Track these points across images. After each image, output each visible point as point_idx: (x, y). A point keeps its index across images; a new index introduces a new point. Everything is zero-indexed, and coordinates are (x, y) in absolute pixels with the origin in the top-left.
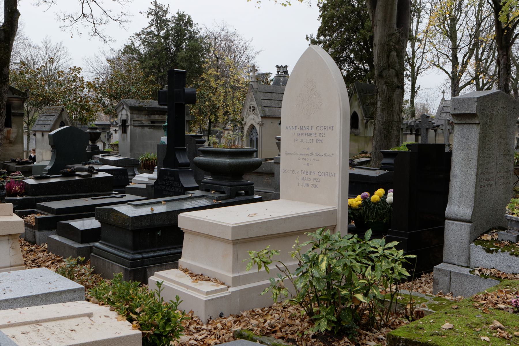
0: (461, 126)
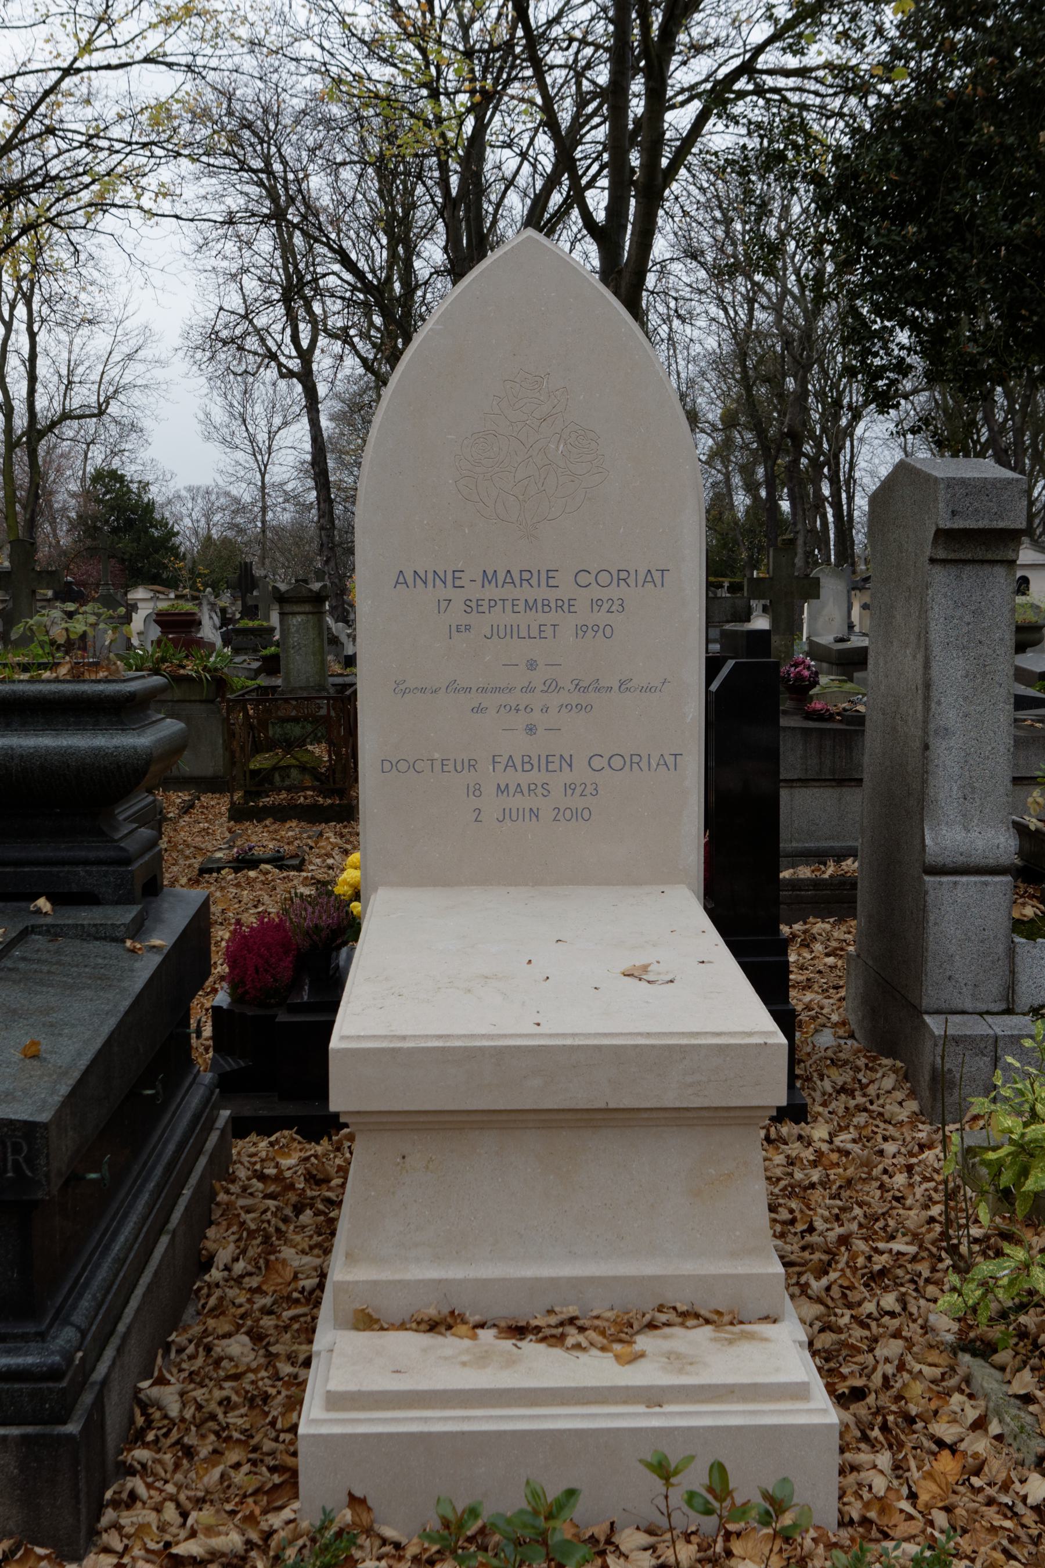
0: (953, 570)
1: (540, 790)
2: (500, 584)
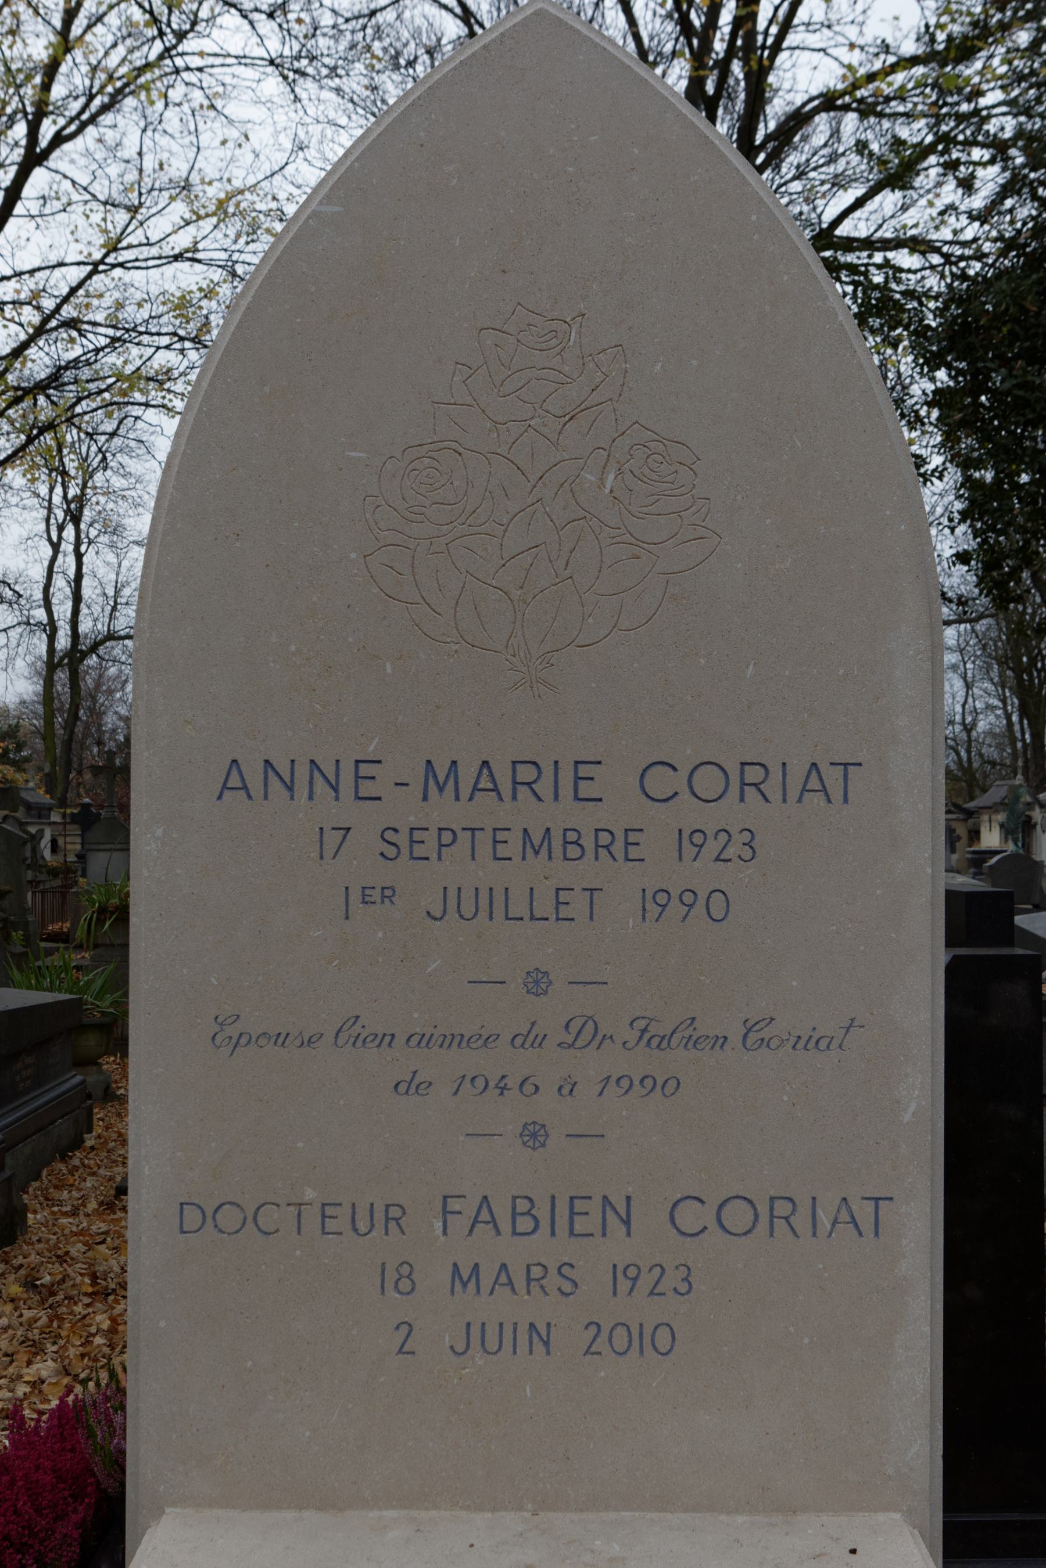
1: (553, 1280)
2: (465, 791)
